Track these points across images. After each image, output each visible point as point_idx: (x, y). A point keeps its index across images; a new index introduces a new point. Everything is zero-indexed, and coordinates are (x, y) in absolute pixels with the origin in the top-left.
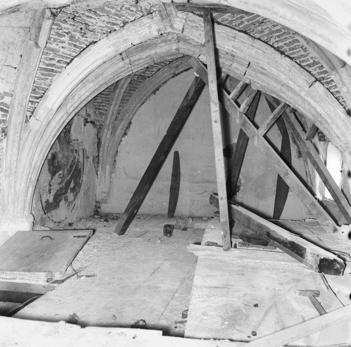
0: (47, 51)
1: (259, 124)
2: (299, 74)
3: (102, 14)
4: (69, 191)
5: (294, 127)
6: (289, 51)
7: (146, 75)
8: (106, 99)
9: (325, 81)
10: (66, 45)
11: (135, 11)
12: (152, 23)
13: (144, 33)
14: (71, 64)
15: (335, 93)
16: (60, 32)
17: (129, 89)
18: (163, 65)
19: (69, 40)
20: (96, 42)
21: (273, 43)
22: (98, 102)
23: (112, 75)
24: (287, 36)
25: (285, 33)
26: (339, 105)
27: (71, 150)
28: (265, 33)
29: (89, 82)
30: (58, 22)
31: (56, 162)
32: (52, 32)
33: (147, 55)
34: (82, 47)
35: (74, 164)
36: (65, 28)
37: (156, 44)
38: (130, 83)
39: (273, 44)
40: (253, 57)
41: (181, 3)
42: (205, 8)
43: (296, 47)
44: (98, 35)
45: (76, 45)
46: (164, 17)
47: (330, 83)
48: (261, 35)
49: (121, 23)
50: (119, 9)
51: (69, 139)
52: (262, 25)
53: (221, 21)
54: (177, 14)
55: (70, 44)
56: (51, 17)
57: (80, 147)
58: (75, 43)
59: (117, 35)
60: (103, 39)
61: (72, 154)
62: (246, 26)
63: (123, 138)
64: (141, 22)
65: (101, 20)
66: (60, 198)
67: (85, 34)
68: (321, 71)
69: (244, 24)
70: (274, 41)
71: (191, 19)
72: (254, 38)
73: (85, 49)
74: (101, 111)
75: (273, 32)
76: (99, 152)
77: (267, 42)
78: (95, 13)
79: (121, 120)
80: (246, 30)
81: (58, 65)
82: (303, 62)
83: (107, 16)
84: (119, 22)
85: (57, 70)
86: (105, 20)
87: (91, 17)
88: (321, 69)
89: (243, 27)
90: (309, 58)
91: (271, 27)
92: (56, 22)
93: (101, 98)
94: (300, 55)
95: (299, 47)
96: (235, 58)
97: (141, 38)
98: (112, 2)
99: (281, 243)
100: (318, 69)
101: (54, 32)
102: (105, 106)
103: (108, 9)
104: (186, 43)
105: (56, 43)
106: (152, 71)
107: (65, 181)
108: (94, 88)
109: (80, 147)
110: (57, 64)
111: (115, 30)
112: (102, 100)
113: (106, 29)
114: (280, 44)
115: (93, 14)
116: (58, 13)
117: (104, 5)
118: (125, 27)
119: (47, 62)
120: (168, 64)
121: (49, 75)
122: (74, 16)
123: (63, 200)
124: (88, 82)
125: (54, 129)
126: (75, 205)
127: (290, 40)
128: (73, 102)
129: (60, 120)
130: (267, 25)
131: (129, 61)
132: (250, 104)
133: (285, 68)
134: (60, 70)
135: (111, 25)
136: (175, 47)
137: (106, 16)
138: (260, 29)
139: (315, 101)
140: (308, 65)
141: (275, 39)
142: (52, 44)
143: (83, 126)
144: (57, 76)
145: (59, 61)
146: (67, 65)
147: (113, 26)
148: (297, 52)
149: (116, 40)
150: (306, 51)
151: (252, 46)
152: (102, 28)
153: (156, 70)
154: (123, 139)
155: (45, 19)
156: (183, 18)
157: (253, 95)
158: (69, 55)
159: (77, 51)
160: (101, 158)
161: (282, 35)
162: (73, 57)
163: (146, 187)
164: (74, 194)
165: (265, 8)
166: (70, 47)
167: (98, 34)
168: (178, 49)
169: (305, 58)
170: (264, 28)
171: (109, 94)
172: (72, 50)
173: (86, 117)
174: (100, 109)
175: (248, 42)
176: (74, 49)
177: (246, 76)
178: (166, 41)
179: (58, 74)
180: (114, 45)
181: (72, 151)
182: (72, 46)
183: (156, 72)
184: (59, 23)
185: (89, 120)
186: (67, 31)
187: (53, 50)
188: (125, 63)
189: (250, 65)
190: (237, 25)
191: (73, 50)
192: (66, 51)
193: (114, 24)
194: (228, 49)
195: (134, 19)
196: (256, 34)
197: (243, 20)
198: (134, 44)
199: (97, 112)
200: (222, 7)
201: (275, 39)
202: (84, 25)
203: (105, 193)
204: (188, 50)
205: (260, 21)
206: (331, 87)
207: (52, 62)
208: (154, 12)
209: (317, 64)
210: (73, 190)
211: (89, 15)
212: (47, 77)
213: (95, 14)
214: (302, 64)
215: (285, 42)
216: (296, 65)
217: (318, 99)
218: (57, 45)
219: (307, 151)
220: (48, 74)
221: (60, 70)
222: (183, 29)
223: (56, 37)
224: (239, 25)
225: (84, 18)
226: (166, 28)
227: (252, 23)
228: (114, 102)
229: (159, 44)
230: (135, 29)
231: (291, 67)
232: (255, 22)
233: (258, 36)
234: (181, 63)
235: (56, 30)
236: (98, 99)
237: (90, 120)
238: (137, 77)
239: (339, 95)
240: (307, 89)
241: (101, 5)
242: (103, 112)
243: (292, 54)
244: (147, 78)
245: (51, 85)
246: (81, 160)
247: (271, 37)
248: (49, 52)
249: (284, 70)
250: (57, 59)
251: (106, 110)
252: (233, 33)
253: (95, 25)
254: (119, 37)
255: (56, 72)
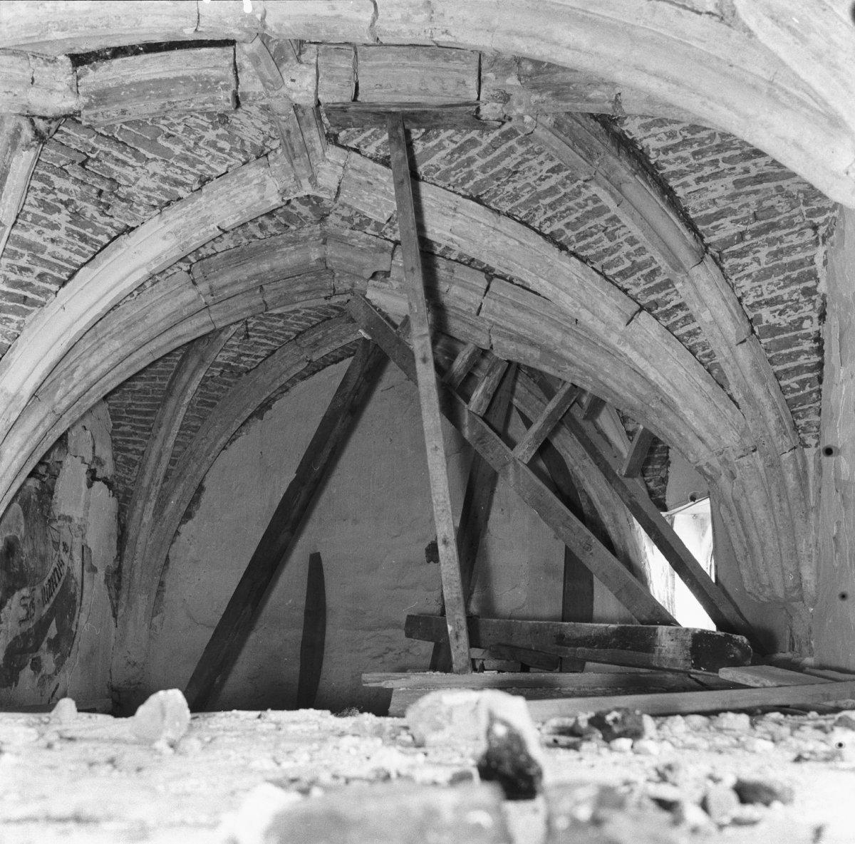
0: (14, 248)
1: (516, 437)
2: (603, 295)
3: (150, 156)
4: (44, 645)
5: (596, 449)
6: (578, 242)
7: (242, 365)
8: (144, 426)
9: (660, 309)
10: (61, 233)
11: (227, 151)
12: (267, 176)
13: (249, 201)
14: (70, 284)
15: (685, 338)
16: (50, 198)
17: (201, 393)
18: (283, 342)
19: (70, 222)
20: (133, 229)
21: (540, 223)
22: (123, 433)
23: (168, 319)
24: (571, 204)
25: (565, 195)
26: (696, 364)
27: (54, 542)
28: (523, 199)
29: (112, 337)
30: (44, 172)
31: (16, 562)
32: (31, 198)
33: (251, 273)
34: (98, 242)
35: (59, 579)
36: (60, 190)
37: (272, 249)
38: (202, 385)
39: (540, 227)
40: (497, 255)
41: (338, 103)
42: (390, 112)
43: (593, 230)
44: (139, 211)
45: (85, 235)
46: (297, 149)
47: (673, 313)
48: (512, 205)
49: (195, 181)
50: (192, 144)
51: (49, 512)
52: (516, 178)
53: (423, 172)
54: (326, 154)
55: (70, 233)
56: (35, 143)
57: (75, 540)
58: (82, 231)
59: (184, 209)
60: (152, 221)
61: (55, 552)
62: (478, 186)
63: (183, 526)
64: (244, 176)
65: (148, 172)
66: (20, 660)
67: (108, 207)
68: (651, 285)
69: (475, 180)
70: (542, 220)
71: (358, 167)
72: (498, 212)
73: (106, 246)
74: (129, 455)
75: (538, 197)
76: (121, 561)
77: (528, 221)
78: (135, 153)
79: (180, 478)
80: (480, 194)
81: (39, 286)
82: (608, 266)
83: (164, 160)
84: (190, 178)
85: (36, 297)
86: (158, 172)
87: (125, 163)
88: (651, 281)
89: (472, 187)
90: (622, 256)
91: (535, 182)
92: (40, 172)
93: (131, 421)
94: (601, 249)
95: (599, 231)
96: (456, 276)
97: (241, 212)
98: (181, 104)
99: (595, 644)
100: (642, 281)
101: (36, 199)
102: (140, 442)
103: (166, 144)
104: (343, 245)
105: (38, 228)
106: (257, 357)
107: (36, 618)
108: (122, 352)
109: (75, 540)
110: (37, 283)
111: (179, 199)
112: (133, 427)
113: (158, 195)
114: (558, 225)
115: (130, 155)
116: (52, 131)
117: (163, 110)
118: (204, 190)
119: (13, 277)
120: (295, 339)
121: (15, 311)
122: (85, 157)
123: (29, 666)
124: (107, 337)
125: (19, 452)
126: (58, 686)
127: (578, 215)
128: (70, 387)
129: (35, 429)
130: (526, 178)
131: (208, 288)
132: (491, 394)
133: (570, 279)
134: (43, 299)
135: (171, 185)
136: (317, 256)
137: (160, 163)
138: (512, 191)
139: (642, 355)
140: (621, 274)
141: (545, 213)
142: (27, 230)
143: (84, 486)
144: (34, 314)
145: (41, 277)
146: (60, 287)
147: (175, 189)
148: (594, 243)
149: (182, 221)
150: (615, 239)
151: (494, 229)
152: (149, 194)
153: (264, 354)
154: (184, 528)
155: (18, 148)
156: (339, 164)
157: (499, 371)
158: (67, 261)
159: (86, 252)
160: (126, 576)
161: (560, 201)
162: (76, 265)
163: (245, 614)
164: (56, 657)
165: (533, 36)
166: (70, 239)
167: (141, 208)
168: (325, 259)
169: (612, 258)
170: (519, 186)
171: (150, 412)
172: (75, 248)
173: (93, 467)
174: (128, 450)
175: (487, 222)
176: (79, 246)
177: (482, 314)
178: (294, 241)
179: (36, 310)
180: (176, 234)
181: (56, 544)
182: (74, 238)
183: (266, 359)
184: (50, 174)
185: (99, 475)
186: (65, 198)
187: (29, 246)
188: (200, 293)
189: (490, 290)
190: (460, 181)
191: (76, 247)
192: (59, 250)
193: (177, 183)
194: (440, 235)
195: (224, 171)
196: (501, 204)
197: (474, 167)
198: (226, 226)
199: (119, 459)
200: (428, 109)
201: (545, 213)
202: (108, 183)
203: (135, 664)
204: (348, 261)
205: (510, 170)
206: (676, 323)
207: (26, 278)
208: (273, 152)
209: (640, 269)
210: (54, 645)
211: (121, 156)
212: (10, 316)
213: (134, 155)
214: (607, 272)
215: (566, 220)
216: (594, 273)
217: (647, 351)
218: (40, 233)
219: (630, 501)
220: (13, 307)
221: (43, 299)
222: (339, 188)
223: (39, 212)
224: (465, 181)
225: (108, 164)
226: (300, 187)
227: (492, 175)
228: (163, 430)
229: (280, 247)
230: (227, 193)
231: (583, 277)
232: (500, 172)
233: (506, 207)
234: (325, 335)
235: (39, 192)
236: (124, 425)
237: (104, 475)
238: (219, 369)
239: (696, 341)
240: (622, 327)
241: (155, 111)
242: (136, 457)
243: (583, 248)
244: (244, 374)
245: (18, 336)
246: (77, 571)
247: (536, 210)
248: (20, 251)
249: (568, 286)
250: (38, 270)
251: (143, 453)
252: (451, 201)
253: (134, 184)
254: (188, 213)
255: (34, 303)
